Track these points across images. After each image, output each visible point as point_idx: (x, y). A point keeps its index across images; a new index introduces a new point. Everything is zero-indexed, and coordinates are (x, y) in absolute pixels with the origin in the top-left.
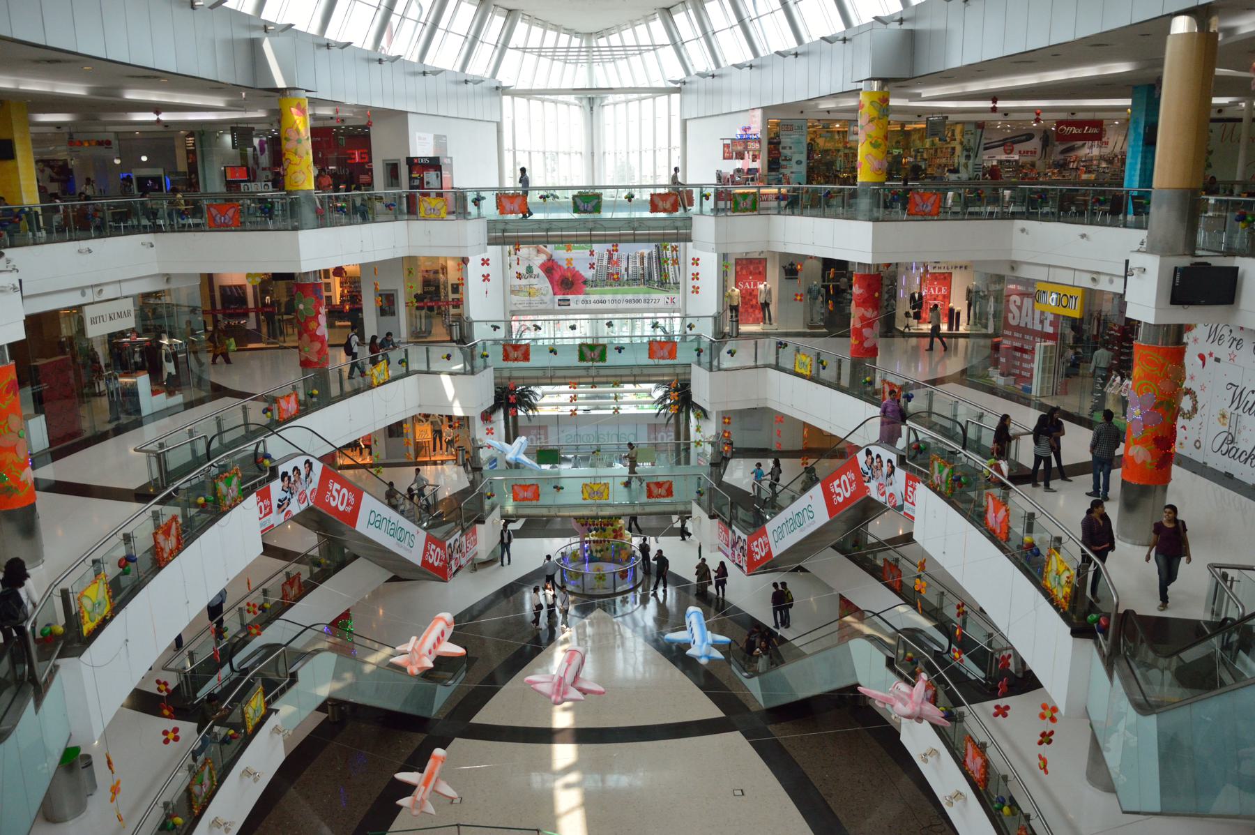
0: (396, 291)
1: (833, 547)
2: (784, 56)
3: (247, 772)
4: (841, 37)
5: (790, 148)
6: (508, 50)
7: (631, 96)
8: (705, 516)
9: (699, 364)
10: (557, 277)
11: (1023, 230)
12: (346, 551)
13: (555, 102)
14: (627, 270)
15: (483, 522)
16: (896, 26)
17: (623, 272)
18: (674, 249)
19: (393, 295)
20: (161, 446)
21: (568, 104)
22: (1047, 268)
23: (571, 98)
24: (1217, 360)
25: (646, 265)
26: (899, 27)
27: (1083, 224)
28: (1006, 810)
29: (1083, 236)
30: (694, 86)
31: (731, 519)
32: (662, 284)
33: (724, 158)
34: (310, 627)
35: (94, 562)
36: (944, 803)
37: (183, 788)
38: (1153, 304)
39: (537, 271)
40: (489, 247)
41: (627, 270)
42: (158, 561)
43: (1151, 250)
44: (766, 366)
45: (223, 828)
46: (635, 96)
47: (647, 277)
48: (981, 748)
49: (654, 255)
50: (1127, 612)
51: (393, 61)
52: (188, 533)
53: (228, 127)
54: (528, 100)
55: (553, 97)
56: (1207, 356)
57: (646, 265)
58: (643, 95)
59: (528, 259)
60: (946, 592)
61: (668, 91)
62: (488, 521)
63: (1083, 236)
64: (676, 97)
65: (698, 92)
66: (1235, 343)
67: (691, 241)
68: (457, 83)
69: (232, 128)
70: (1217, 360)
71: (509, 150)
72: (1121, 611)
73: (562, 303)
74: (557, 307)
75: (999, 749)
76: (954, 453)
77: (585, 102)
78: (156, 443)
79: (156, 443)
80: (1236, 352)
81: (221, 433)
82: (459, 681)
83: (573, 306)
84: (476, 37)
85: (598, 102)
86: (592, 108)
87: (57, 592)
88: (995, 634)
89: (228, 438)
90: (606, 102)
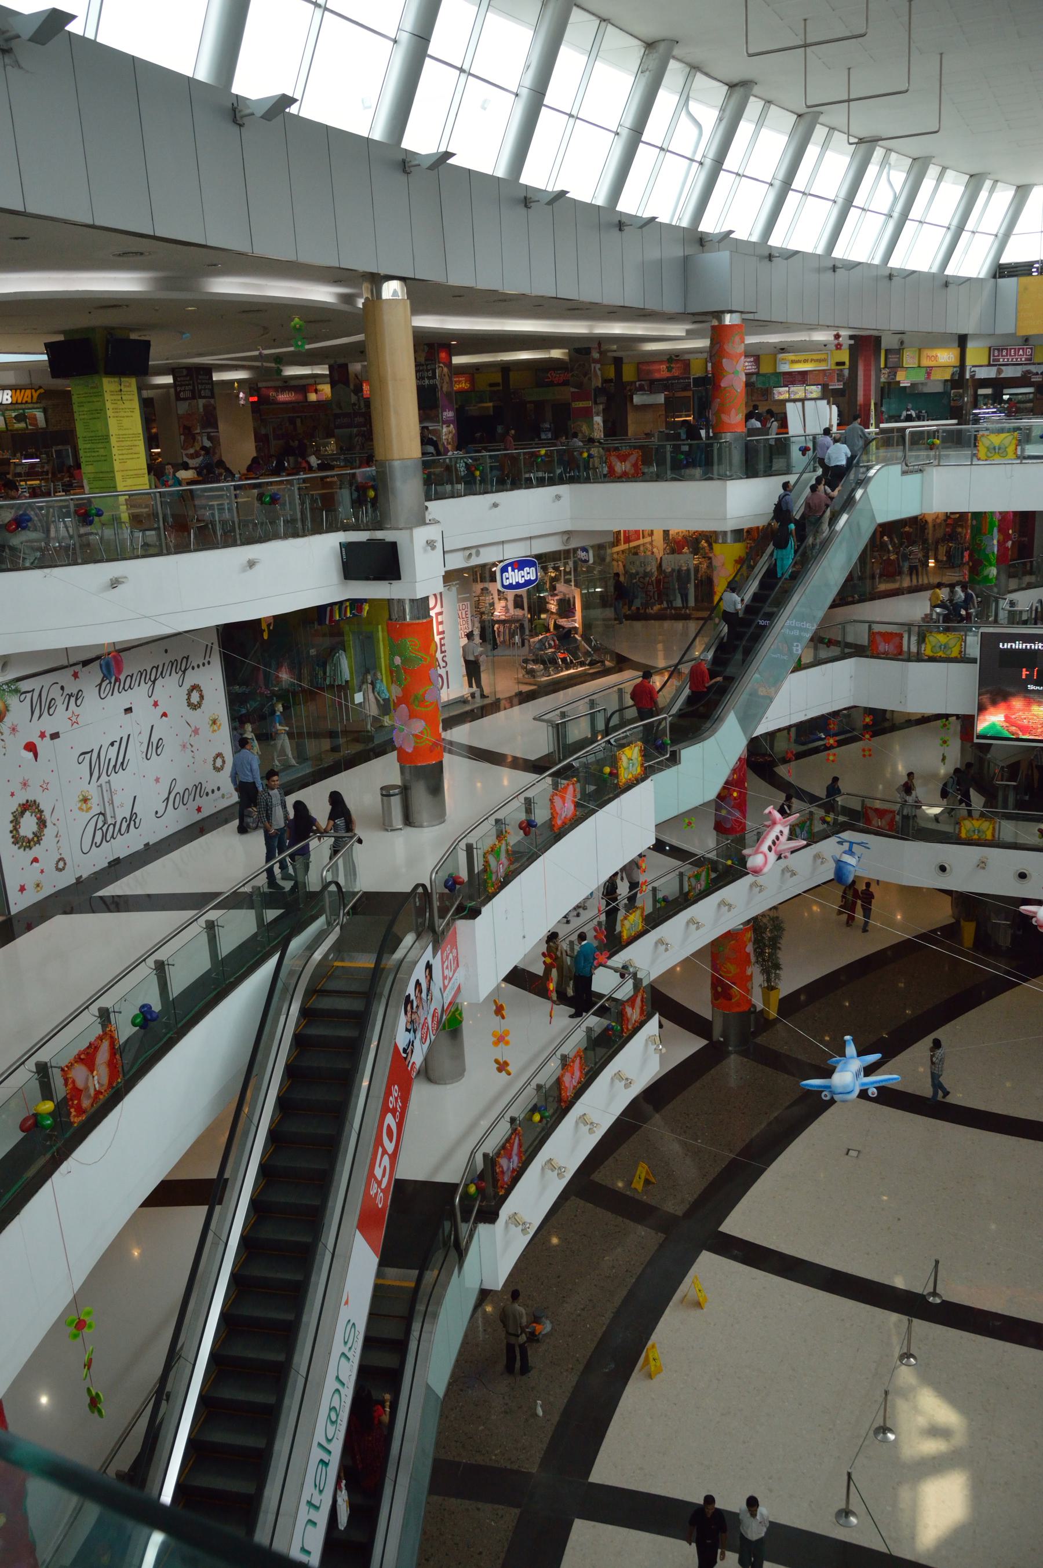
3: (618, 1075)
20: (563, 715)
24: (55, 736)
33: (639, 363)
35: (497, 821)
37: (554, 1079)
38: (712, 739)
42: (557, 832)
52: (584, 812)
56: (37, 741)
66: (73, 699)
70: (55, 736)
78: (558, 712)
79: (558, 712)
80: (77, 710)
87: (463, 845)
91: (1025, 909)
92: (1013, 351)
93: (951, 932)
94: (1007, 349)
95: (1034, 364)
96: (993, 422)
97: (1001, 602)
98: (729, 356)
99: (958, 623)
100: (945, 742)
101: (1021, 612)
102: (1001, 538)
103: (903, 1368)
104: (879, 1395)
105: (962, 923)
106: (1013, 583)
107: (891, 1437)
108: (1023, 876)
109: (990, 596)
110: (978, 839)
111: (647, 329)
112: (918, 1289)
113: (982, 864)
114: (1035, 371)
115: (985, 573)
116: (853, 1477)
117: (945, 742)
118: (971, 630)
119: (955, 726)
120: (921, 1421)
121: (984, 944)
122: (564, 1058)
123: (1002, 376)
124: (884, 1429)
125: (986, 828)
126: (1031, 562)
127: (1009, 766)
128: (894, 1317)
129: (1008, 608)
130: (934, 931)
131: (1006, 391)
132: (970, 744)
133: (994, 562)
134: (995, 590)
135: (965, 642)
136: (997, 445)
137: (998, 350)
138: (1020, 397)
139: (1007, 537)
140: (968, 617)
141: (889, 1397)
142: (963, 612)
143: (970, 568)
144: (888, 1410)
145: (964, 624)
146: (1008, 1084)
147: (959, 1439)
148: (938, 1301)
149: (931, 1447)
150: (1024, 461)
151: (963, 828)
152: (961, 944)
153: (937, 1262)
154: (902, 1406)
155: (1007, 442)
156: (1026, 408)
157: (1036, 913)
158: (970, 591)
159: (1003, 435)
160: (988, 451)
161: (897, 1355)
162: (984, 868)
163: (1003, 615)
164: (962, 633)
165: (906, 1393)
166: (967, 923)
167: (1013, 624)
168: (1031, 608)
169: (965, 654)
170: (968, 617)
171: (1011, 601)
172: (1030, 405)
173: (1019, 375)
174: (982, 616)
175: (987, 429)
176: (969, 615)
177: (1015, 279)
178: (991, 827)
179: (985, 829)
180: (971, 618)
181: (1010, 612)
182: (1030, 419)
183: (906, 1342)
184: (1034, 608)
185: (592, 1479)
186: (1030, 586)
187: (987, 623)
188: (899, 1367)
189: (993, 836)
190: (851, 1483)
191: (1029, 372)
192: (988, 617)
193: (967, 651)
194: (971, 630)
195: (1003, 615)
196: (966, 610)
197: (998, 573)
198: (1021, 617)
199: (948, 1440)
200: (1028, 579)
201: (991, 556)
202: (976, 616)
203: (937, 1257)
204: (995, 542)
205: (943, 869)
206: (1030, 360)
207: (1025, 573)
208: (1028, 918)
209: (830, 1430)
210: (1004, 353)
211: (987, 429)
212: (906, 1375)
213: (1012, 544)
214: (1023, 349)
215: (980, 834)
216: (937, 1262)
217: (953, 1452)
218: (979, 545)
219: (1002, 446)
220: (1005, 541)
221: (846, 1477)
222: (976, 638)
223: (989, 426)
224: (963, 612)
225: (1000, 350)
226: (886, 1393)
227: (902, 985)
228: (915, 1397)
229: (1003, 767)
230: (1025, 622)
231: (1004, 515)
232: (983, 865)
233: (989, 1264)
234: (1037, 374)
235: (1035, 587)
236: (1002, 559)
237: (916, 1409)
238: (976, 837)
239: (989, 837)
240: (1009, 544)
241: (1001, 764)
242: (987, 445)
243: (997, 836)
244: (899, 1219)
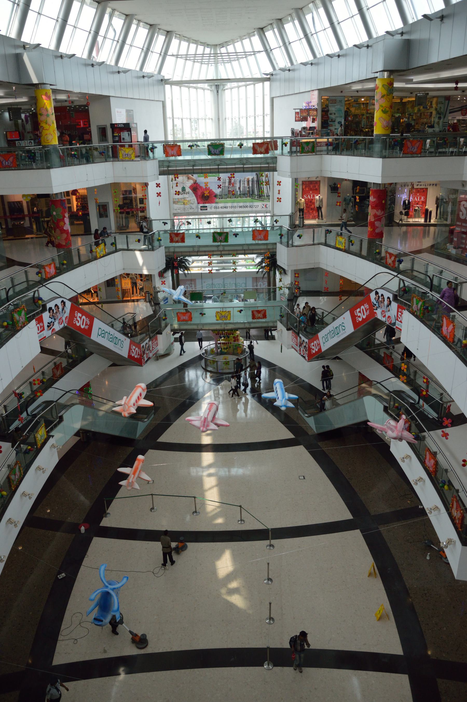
0: (108, 203)
1: (356, 346)
5: (335, 114)
6: (168, 56)
7: (241, 84)
8: (284, 329)
9: (281, 243)
10: (199, 193)
12: (86, 350)
13: (196, 88)
14: (239, 188)
15: (161, 334)
16: (398, 37)
17: (237, 189)
19: (106, 205)
21: (204, 89)
23: (206, 86)
25: (250, 185)
28: (446, 487)
30: (278, 77)
31: (299, 331)
32: (260, 196)
34: (68, 392)
39: (188, 190)
40: (160, 176)
41: (239, 188)
44: (319, 244)
45: (28, 497)
46: (243, 83)
47: (251, 192)
49: (255, 179)
51: (70, 58)
53: (6, 108)
54: (180, 87)
55: (194, 85)
57: (250, 185)
58: (248, 83)
59: (183, 183)
60: (418, 371)
61: (262, 80)
62: (164, 333)
64: (267, 84)
65: (280, 80)
67: (277, 171)
68: (138, 77)
69: (8, 108)
71: (170, 118)
73: (203, 208)
74: (200, 211)
75: (444, 455)
77: (214, 88)
81: (13, 286)
82: (150, 419)
83: (209, 210)
84: (148, 49)
85: (221, 87)
86: (218, 92)
88: (444, 394)
89: (18, 289)
90: (226, 87)
98: (41, 115)
122: (9, 466)
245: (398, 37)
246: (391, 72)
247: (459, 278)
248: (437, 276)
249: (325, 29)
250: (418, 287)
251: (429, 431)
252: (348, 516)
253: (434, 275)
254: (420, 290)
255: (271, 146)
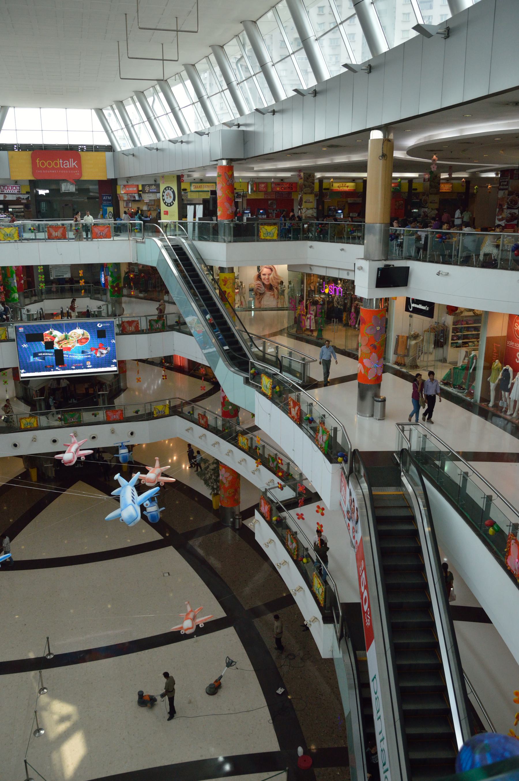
2: (264, 114)
4: (180, 140)
11: (311, 247)
16: (235, 128)
18: (264, 275)
22: (338, 271)
26: (237, 129)
27: (291, 241)
28: (305, 560)
29: (342, 250)
36: (276, 567)
43: (366, 258)
48: (294, 535)
50: (354, 450)
60: (266, 445)
63: (342, 250)
72: (352, 450)
75: (303, 534)
76: (276, 374)
91: (57, 456)
92: (10, 187)
93: (25, 475)
94: (7, 186)
95: (21, 194)
96: (6, 222)
97: (23, 310)
99: (3, 322)
100: (6, 382)
101: (33, 314)
102: (18, 279)
103: (42, 696)
104: (32, 715)
105: (30, 470)
106: (27, 301)
107: (42, 732)
108: (54, 441)
109: (17, 308)
110: (31, 428)
111: (509, 125)
112: (41, 655)
113: (34, 440)
114: (22, 197)
115: (13, 296)
116: (27, 761)
117: (6, 382)
118: (10, 325)
119: (10, 372)
120: (56, 717)
121: (42, 478)
123: (7, 199)
124: (38, 730)
125: (33, 422)
126: (35, 290)
127: (39, 390)
128: (32, 673)
129: (26, 313)
130: (17, 477)
131: (9, 207)
132: (19, 382)
133: (16, 291)
134: (19, 304)
135: (8, 331)
136: (8, 233)
137: (3, 186)
138: (17, 210)
139: (21, 279)
140: (7, 319)
141: (37, 713)
142: (4, 317)
143: (5, 294)
144: (38, 720)
145: (6, 322)
146: (66, 542)
147: (75, 718)
148: (52, 656)
149: (63, 727)
150: (23, 241)
151: (22, 424)
152: (31, 481)
153: (48, 638)
154: (45, 715)
155: (13, 232)
156: (21, 216)
157: (62, 457)
158: (7, 306)
159: (11, 228)
160: (4, 236)
161: (37, 691)
162: (35, 441)
163: (24, 317)
164: (5, 327)
165: (45, 708)
166: (32, 470)
167: (30, 320)
168: (37, 312)
169: (8, 337)
170: (7, 319)
171: (27, 310)
172: (22, 214)
173: (15, 199)
174: (14, 317)
175: (3, 225)
176: (7, 318)
177: (6, 152)
178: (35, 420)
179: (33, 422)
180: (9, 319)
181: (27, 315)
182: (24, 221)
183: (40, 683)
184: (39, 312)
185: (225, 615)
186: (35, 302)
187: (17, 321)
188: (40, 696)
189: (37, 424)
190: (27, 765)
191: (20, 198)
192: (17, 318)
193: (9, 336)
194: (10, 325)
195: (24, 317)
196: (6, 315)
197: (19, 296)
198: (33, 318)
199: (69, 720)
200: (34, 298)
201: (14, 288)
202: (12, 318)
203: (47, 636)
204: (15, 281)
205: (15, 445)
206: (19, 192)
207: (32, 296)
208: (59, 461)
209: (11, 744)
210: (6, 188)
211: (3, 225)
212: (44, 699)
213: (24, 282)
214: (15, 186)
215: (31, 425)
216: (48, 638)
217: (73, 724)
218: (7, 283)
219: (11, 234)
220: (20, 280)
221: (24, 763)
222: (13, 329)
223: (4, 224)
224: (4, 317)
225: (4, 186)
226: (36, 712)
227: (5, 508)
228: (50, 708)
229: (36, 391)
230: (36, 319)
231: (17, 268)
232: (35, 440)
233: (72, 629)
234: (24, 199)
235: (39, 302)
236: (19, 289)
237: (52, 713)
238: (29, 427)
239: (35, 425)
240: (22, 282)
241: (35, 389)
242: (3, 233)
243: (39, 424)
244: (25, 625)
245: (235, 128)
246: (230, 161)
247: (306, 358)
248: (285, 357)
249: (193, 104)
250: (267, 368)
251: (288, 510)
252: (221, 614)
253: (282, 357)
254: (269, 371)
255: (170, 227)
